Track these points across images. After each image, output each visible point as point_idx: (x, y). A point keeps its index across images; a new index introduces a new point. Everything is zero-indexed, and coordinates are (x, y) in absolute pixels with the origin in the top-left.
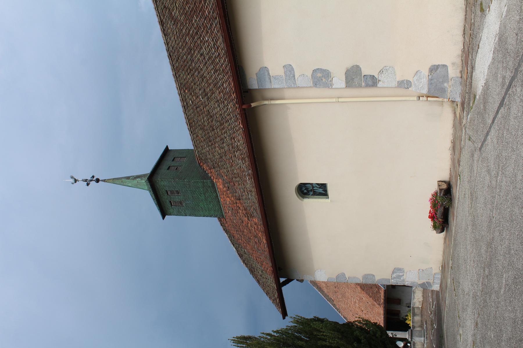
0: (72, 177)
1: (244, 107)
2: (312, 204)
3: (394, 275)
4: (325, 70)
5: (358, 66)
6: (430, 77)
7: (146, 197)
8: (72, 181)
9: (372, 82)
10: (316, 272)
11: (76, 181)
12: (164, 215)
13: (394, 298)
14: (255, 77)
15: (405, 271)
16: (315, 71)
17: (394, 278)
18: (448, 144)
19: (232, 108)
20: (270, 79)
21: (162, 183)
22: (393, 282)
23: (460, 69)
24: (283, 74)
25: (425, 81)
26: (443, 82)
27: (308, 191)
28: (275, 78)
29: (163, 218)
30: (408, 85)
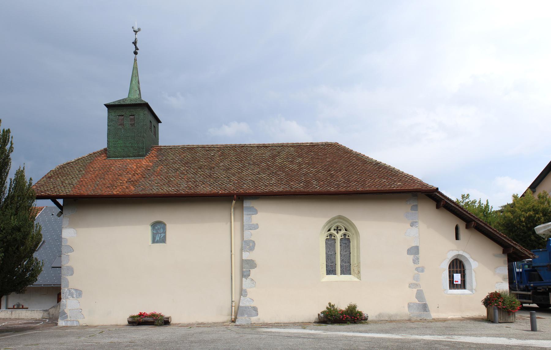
0: (139, 30)
1: (235, 196)
2: (146, 231)
3: (73, 291)
4: (254, 248)
5: (256, 267)
7: (120, 95)
8: (136, 29)
9: (244, 275)
11: (136, 32)
12: (109, 107)
13: (55, 292)
15: (78, 299)
16: (254, 242)
17: (70, 291)
18: (200, 321)
19: (231, 188)
21: (142, 114)
23: (256, 323)
25: (248, 304)
26: (247, 314)
27: (156, 230)
29: (106, 105)
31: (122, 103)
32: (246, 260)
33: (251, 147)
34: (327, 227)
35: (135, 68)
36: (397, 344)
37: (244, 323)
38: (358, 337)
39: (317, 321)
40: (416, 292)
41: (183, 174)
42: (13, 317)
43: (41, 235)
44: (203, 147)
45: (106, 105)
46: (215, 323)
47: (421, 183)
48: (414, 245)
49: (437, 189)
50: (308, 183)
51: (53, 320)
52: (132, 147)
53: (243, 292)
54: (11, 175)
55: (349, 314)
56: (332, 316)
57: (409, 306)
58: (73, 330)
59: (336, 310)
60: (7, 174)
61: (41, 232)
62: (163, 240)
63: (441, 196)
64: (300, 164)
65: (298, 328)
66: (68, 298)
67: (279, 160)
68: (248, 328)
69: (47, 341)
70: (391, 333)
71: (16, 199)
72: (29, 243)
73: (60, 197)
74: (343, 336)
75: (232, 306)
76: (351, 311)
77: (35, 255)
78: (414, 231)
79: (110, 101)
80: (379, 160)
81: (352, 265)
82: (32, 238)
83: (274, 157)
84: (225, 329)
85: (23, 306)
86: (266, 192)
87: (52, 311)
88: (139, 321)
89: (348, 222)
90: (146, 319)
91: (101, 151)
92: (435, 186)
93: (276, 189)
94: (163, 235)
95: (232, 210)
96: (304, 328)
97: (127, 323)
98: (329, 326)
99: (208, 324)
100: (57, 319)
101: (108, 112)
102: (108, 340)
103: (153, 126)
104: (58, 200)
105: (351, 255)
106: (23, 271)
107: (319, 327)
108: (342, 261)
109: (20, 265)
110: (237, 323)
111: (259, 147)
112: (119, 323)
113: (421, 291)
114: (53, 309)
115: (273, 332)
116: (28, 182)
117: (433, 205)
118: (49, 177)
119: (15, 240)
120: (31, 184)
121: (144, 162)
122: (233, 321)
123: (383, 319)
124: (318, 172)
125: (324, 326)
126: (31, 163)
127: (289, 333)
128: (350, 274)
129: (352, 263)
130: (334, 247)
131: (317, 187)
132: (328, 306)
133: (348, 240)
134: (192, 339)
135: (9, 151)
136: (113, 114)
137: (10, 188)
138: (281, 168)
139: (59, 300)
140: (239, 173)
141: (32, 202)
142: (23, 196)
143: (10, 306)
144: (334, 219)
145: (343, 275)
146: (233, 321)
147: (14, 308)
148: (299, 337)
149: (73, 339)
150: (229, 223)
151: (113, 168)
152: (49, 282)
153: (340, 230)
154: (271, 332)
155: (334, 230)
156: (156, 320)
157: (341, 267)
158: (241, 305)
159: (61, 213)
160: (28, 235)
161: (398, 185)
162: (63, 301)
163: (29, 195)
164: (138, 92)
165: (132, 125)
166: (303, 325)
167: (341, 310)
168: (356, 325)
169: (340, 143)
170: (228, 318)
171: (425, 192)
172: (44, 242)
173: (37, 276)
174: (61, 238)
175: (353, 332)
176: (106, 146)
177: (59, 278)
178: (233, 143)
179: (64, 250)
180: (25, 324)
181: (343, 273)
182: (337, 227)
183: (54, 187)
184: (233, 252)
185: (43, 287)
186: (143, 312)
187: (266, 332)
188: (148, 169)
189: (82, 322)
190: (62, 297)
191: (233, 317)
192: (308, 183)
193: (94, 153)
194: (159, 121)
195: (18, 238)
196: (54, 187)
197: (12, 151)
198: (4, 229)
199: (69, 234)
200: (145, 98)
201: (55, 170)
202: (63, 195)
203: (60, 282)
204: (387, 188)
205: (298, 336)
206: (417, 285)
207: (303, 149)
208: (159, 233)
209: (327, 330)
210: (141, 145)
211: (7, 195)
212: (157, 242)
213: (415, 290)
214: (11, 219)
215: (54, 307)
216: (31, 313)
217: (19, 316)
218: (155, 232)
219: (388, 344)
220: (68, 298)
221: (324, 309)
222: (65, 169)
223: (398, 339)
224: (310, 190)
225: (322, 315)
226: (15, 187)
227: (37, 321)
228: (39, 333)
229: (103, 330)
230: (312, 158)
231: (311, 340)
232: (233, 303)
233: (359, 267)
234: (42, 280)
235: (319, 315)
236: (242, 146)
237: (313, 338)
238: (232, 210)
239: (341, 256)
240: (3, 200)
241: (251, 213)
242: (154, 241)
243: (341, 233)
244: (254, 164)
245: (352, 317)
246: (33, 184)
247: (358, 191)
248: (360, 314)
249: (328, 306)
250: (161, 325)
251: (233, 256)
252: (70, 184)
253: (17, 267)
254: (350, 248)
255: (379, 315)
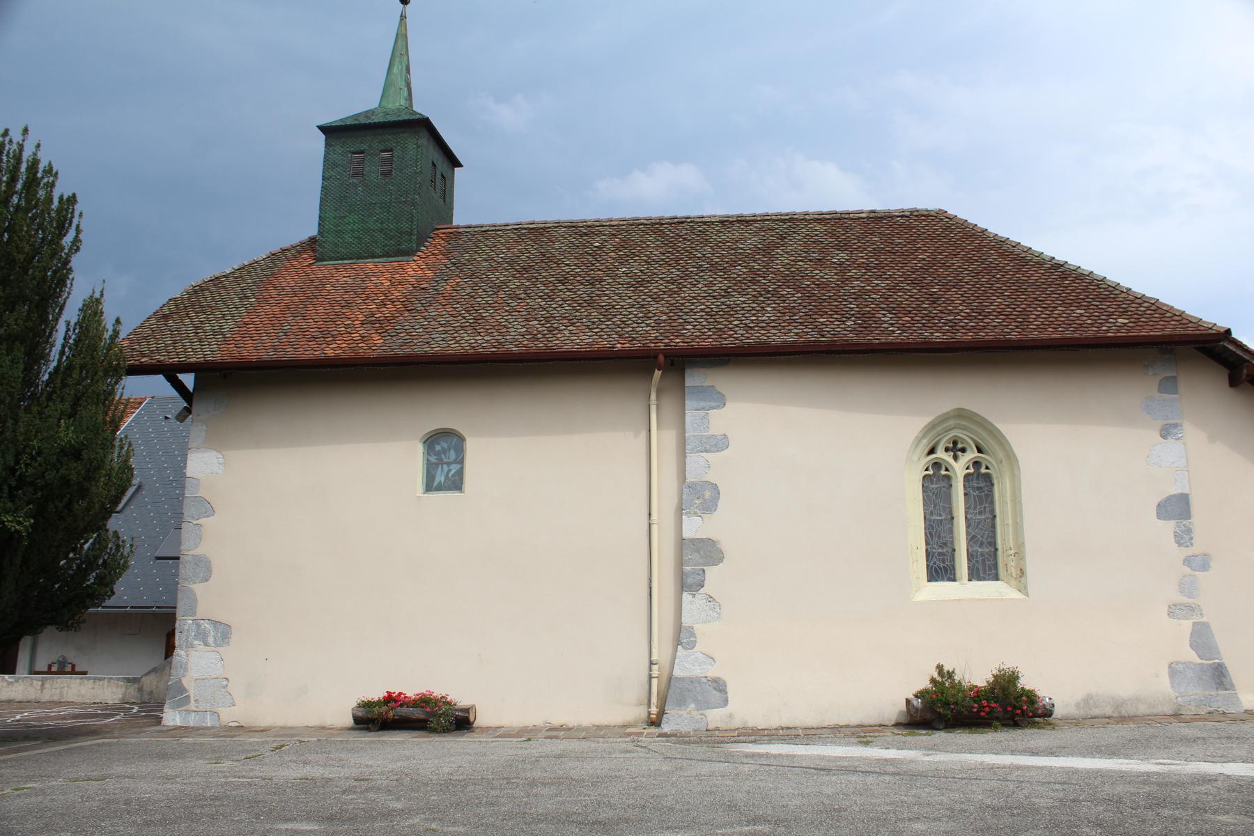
1: (661, 357)
2: (405, 458)
3: (207, 625)
5: (721, 560)
6: (704, 680)
7: (361, 99)
9: (687, 583)
10: (215, 453)
12: (329, 131)
13: (159, 629)
14: (708, 383)
15: (220, 649)
16: (715, 487)
17: (198, 626)
18: (557, 720)
19: (648, 334)
20: (703, 409)
22: (185, 624)
24: (711, 433)
25: (697, 671)
26: (696, 701)
27: (438, 454)
28: (705, 419)
29: (321, 128)
30: (688, 643)
31: (363, 121)
32: (692, 541)
33: (705, 222)
34: (925, 441)
35: (401, 37)
36: (1147, 789)
37: (686, 728)
38: (1028, 768)
39: (903, 720)
40: (1189, 631)
41: (515, 297)
42: (46, 697)
43: (131, 469)
44: (572, 226)
45: (321, 128)
46: (599, 727)
47: (1180, 317)
48: (1175, 490)
49: (1228, 332)
50: (867, 319)
51: (151, 709)
52: (381, 230)
53: (682, 636)
54: (71, 313)
55: (996, 699)
56: (947, 704)
57: (1173, 671)
58: (201, 739)
59: (957, 687)
60: (62, 309)
61: (133, 462)
62: (456, 484)
63: (1239, 352)
64: (842, 268)
65: (848, 744)
66: (192, 646)
67: (782, 258)
68: (699, 742)
69: (128, 770)
70: (1127, 757)
71: (75, 375)
72: (99, 489)
73: (187, 368)
74: (983, 767)
75: (651, 677)
76: (1003, 689)
77: (114, 523)
78: (1170, 451)
79: (330, 118)
80: (1060, 257)
81: (1000, 553)
82: (109, 475)
83: (768, 249)
84: (631, 747)
85: (73, 666)
86: (750, 346)
87: (150, 682)
88: (384, 717)
89: (986, 429)
90: (404, 711)
91: (301, 244)
92: (1222, 323)
93: (776, 337)
94: (455, 468)
95: (653, 396)
96: (867, 744)
97: (350, 721)
98: (940, 736)
99: (580, 729)
100: (160, 706)
101: (326, 144)
102: (294, 772)
103: (438, 174)
104: (181, 377)
105: (998, 520)
106: (79, 566)
107: (909, 738)
108: (971, 539)
109: (74, 550)
110: (666, 728)
111: (726, 223)
112: (328, 722)
113: (1206, 625)
114: (152, 677)
115: (775, 756)
116: (110, 328)
117: (1220, 377)
118: (165, 317)
119: (65, 482)
120: (116, 333)
121: (412, 269)
122: (655, 723)
123: (1097, 712)
124: (895, 288)
125: (923, 737)
126: (119, 279)
127: (822, 758)
128: (997, 578)
129: (999, 546)
130: (948, 498)
131: (891, 329)
132: (936, 675)
133: (988, 478)
134: (537, 774)
135: (71, 249)
136: (339, 149)
137: (63, 347)
138: (791, 279)
139: (170, 649)
140: (671, 293)
141: (116, 383)
142: (100, 362)
143: (41, 665)
144: (944, 419)
145: (975, 583)
146: (655, 723)
147: (49, 672)
148: (854, 771)
149: (201, 765)
150: (644, 434)
151: (328, 287)
152: (146, 600)
153: (963, 450)
154: (767, 755)
155: (947, 450)
156: (433, 714)
157: (970, 556)
158: (677, 672)
159: (188, 411)
160: (98, 468)
161: (1118, 325)
162: (180, 653)
163: (110, 363)
164: (406, 94)
165: (387, 174)
166: (863, 733)
167: (973, 687)
168: (1019, 732)
169: (951, 212)
170: (640, 713)
171: (1195, 342)
172: (139, 487)
173: (113, 582)
174: (184, 475)
175: (1013, 752)
176: (313, 231)
177: (173, 587)
178: (655, 213)
179: (189, 511)
180: (76, 716)
181: (975, 574)
182: (955, 443)
183: (175, 342)
184: (654, 516)
185: (130, 614)
186: (396, 690)
187: (753, 755)
188: (438, 297)
189: (229, 716)
190: (177, 643)
191: (654, 710)
192: (867, 319)
193: (283, 250)
194: (455, 163)
195: (74, 477)
196: (175, 342)
197: (78, 249)
198: (39, 453)
199: (203, 465)
200: (422, 107)
201: (182, 298)
202: (197, 363)
203: (175, 599)
204: (1091, 332)
205: (849, 769)
206: (1192, 609)
207: (850, 228)
208: (444, 464)
209: (934, 748)
210: (405, 226)
211: (55, 364)
212: (440, 488)
213: (1187, 625)
214: (59, 426)
215: (154, 670)
216: (93, 688)
217: (61, 694)
218: (433, 459)
219: (1119, 789)
220: (192, 646)
221: (925, 684)
222: (207, 293)
223: (1149, 774)
224: (874, 337)
225: (918, 703)
226: (77, 342)
227: (108, 710)
228: (110, 745)
229: (286, 741)
230: (877, 252)
231: (887, 778)
232: (654, 667)
233: (1023, 558)
234: (128, 592)
235: (908, 701)
236: (681, 222)
237: (894, 774)
238: (653, 396)
239: (968, 527)
240: (46, 377)
241: (707, 404)
242: (430, 486)
243: (966, 458)
244: (714, 268)
245: (1004, 707)
246: (122, 335)
247: (1009, 341)
248: (1031, 697)
249: (936, 675)
250: (445, 730)
251: (655, 528)
252: (214, 333)
253: (66, 557)
254: (992, 503)
255: (1087, 700)
